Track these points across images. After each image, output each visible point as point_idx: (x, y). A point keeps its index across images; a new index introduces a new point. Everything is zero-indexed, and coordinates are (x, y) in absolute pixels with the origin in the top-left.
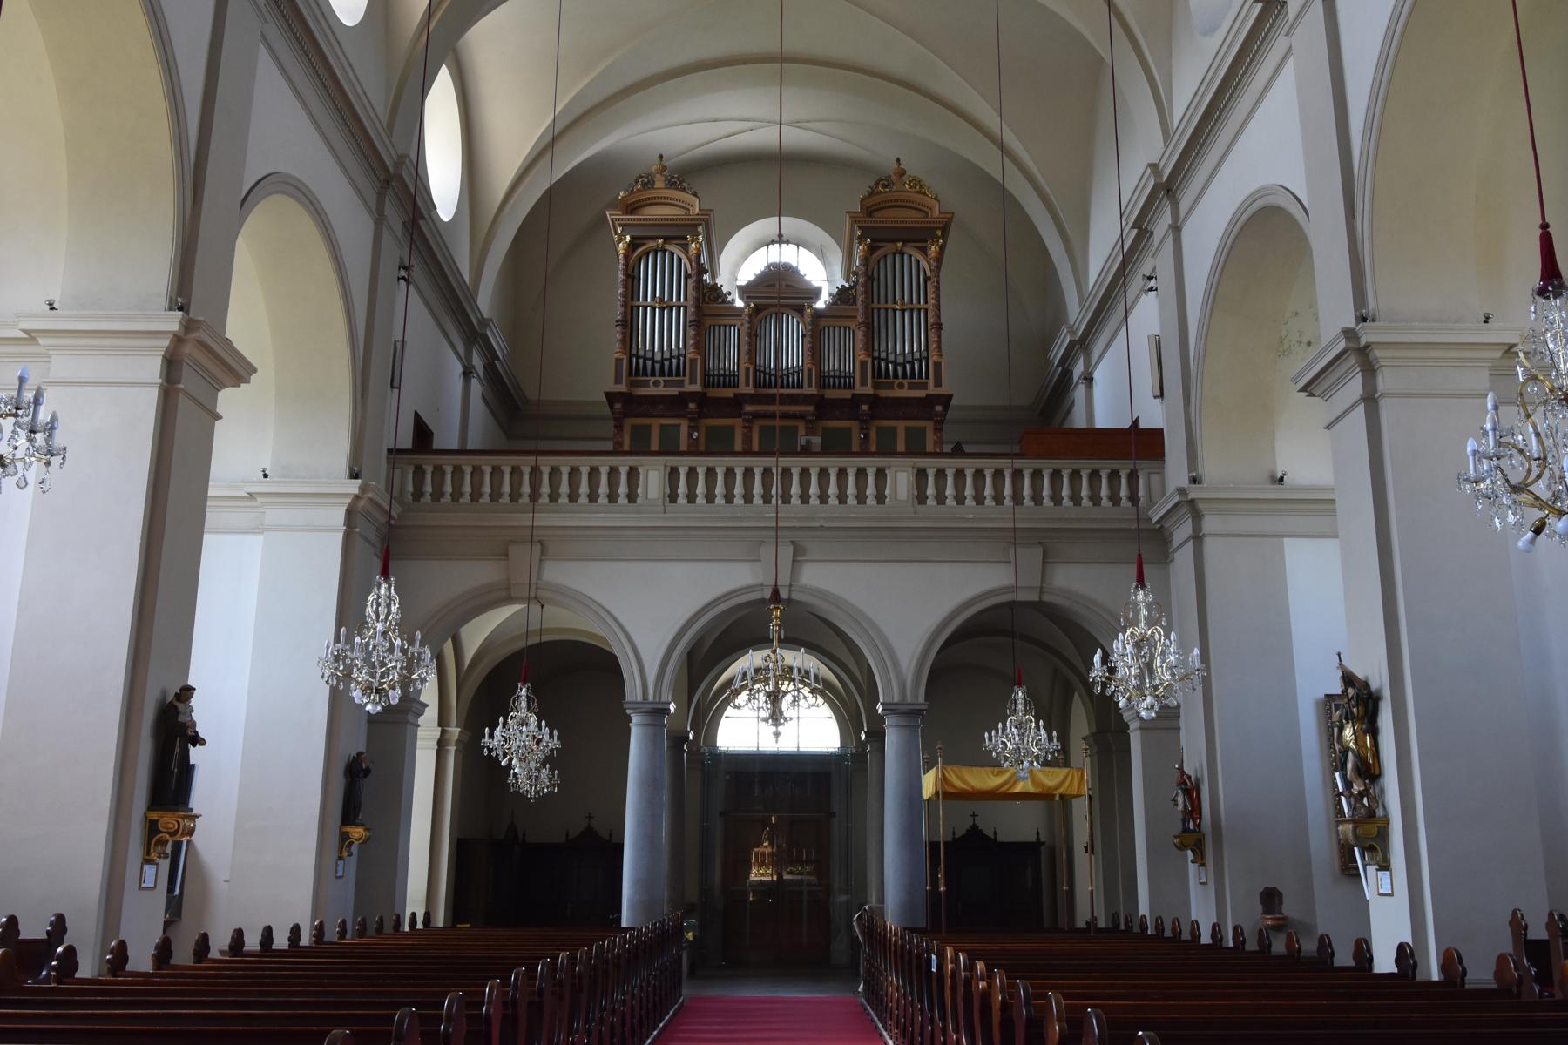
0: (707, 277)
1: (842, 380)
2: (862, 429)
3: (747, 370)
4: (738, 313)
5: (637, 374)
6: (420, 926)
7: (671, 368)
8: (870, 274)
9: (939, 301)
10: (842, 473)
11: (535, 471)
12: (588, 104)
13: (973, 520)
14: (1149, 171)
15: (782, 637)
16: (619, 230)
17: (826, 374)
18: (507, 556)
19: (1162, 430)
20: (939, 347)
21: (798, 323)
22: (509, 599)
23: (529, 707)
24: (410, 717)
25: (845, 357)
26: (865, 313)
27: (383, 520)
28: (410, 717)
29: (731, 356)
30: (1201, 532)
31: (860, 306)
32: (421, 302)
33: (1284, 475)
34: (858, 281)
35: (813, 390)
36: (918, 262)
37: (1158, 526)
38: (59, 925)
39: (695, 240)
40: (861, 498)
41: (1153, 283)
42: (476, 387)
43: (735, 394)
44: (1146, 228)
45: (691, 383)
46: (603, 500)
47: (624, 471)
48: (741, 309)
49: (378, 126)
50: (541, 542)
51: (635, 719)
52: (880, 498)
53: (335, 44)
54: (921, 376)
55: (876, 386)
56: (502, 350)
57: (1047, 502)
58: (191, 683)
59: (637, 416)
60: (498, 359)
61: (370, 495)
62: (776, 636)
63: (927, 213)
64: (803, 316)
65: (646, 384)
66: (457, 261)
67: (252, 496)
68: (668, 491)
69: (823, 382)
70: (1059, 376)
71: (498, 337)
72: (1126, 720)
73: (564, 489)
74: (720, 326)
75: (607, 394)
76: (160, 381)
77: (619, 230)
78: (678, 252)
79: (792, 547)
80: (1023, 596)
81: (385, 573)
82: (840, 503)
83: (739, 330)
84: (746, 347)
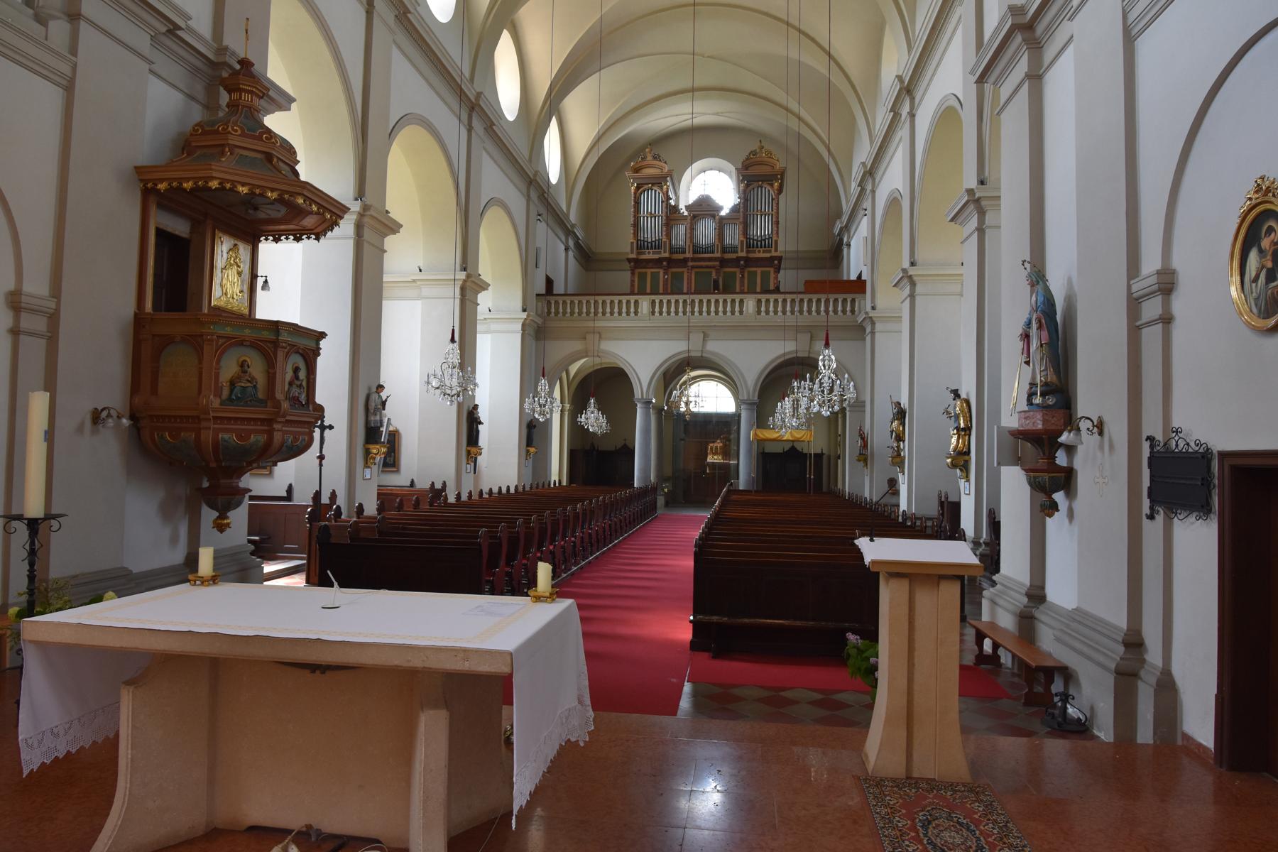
3: (689, 246)
6: (557, 485)
7: (656, 245)
11: (596, 302)
12: (616, 118)
25: (733, 236)
26: (744, 217)
27: (536, 326)
35: (718, 255)
38: (444, 483)
39: (666, 184)
42: (571, 254)
46: (624, 315)
47: (632, 302)
50: (599, 333)
51: (639, 405)
52: (741, 312)
54: (769, 247)
55: (748, 252)
57: (814, 313)
58: (476, 403)
59: (641, 268)
61: (531, 318)
65: (644, 253)
81: (543, 376)
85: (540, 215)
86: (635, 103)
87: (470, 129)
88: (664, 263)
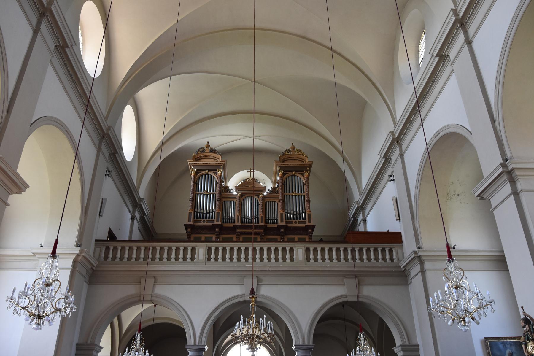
0: (224, 184)
1: (274, 221)
2: (282, 238)
3: (238, 217)
4: (235, 197)
5: (197, 218)
8: (283, 183)
9: (309, 192)
10: (276, 249)
13: (330, 267)
14: (390, 134)
15: (256, 310)
16: (192, 167)
17: (268, 218)
18: (140, 283)
19: (400, 233)
20: (309, 208)
21: (257, 200)
22: (142, 302)
23: (141, 343)
24: (94, 353)
26: (282, 196)
28: (94, 353)
29: (233, 212)
30: (424, 269)
31: (280, 194)
32: (116, 188)
33: (455, 246)
34: (279, 185)
35: (263, 224)
36: (301, 179)
37: (403, 269)
40: (284, 259)
41: (392, 178)
42: (136, 224)
43: (233, 225)
44: (388, 158)
45: (217, 221)
46: (181, 260)
47: (189, 249)
48: (236, 195)
49: (102, 117)
52: (292, 259)
53: (83, 75)
55: (286, 222)
56: (147, 211)
60: (146, 215)
61: (83, 254)
62: (253, 309)
63: (303, 162)
64: (259, 198)
65: (200, 222)
66: (131, 174)
67: (34, 255)
68: (207, 256)
69: (266, 221)
70: (352, 222)
71: (146, 206)
72: (396, 352)
73: (165, 256)
74: (228, 201)
75: (185, 225)
76: (72, 268)
77: (192, 167)
78: (213, 175)
79: (257, 279)
80: (349, 299)
82: (276, 261)
83: (235, 203)
84: (238, 208)
85: (109, 171)
86: (198, 118)
87: (36, 31)
88: (217, 230)
